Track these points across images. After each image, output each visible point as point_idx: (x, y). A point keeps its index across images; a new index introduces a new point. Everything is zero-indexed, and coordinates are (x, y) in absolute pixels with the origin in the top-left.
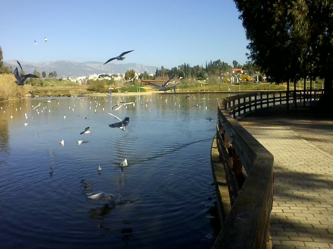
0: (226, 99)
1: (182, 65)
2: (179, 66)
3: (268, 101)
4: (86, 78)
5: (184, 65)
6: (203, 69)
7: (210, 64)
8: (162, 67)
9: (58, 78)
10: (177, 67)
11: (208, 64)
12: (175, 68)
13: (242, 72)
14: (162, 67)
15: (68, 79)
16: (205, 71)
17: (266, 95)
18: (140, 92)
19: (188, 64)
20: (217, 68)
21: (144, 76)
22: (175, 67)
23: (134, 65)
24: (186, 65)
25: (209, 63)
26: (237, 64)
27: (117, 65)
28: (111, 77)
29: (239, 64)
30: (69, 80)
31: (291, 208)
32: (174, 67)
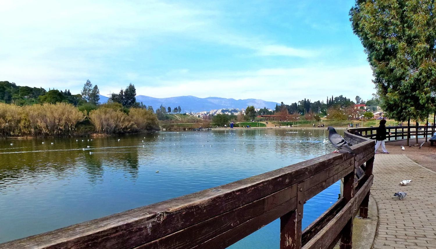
0: (362, 41)
1: (303, 101)
2: (299, 102)
4: (208, 113)
5: (304, 100)
7: (331, 100)
8: (282, 103)
9: (182, 113)
10: (297, 103)
11: (329, 99)
12: (296, 104)
13: (365, 108)
14: (282, 103)
15: (191, 114)
18: (224, 131)
19: (308, 100)
20: (339, 105)
21: (265, 111)
22: (296, 103)
23: (253, 101)
24: (307, 100)
25: (330, 99)
26: (165, 109)
27: (236, 100)
28: (230, 112)
30: (192, 115)
32: (294, 102)
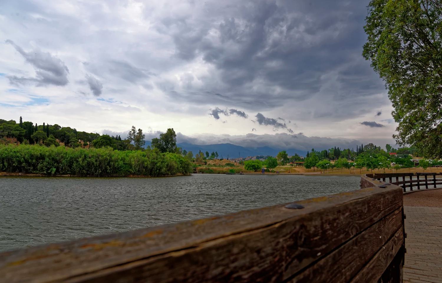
3: (411, 184)
5: (334, 148)
6: (354, 153)
11: (359, 148)
14: (313, 150)
16: (185, 161)
17: (433, 176)
19: (338, 148)
24: (337, 148)
25: (360, 147)
29: (393, 148)
31: (423, 251)
